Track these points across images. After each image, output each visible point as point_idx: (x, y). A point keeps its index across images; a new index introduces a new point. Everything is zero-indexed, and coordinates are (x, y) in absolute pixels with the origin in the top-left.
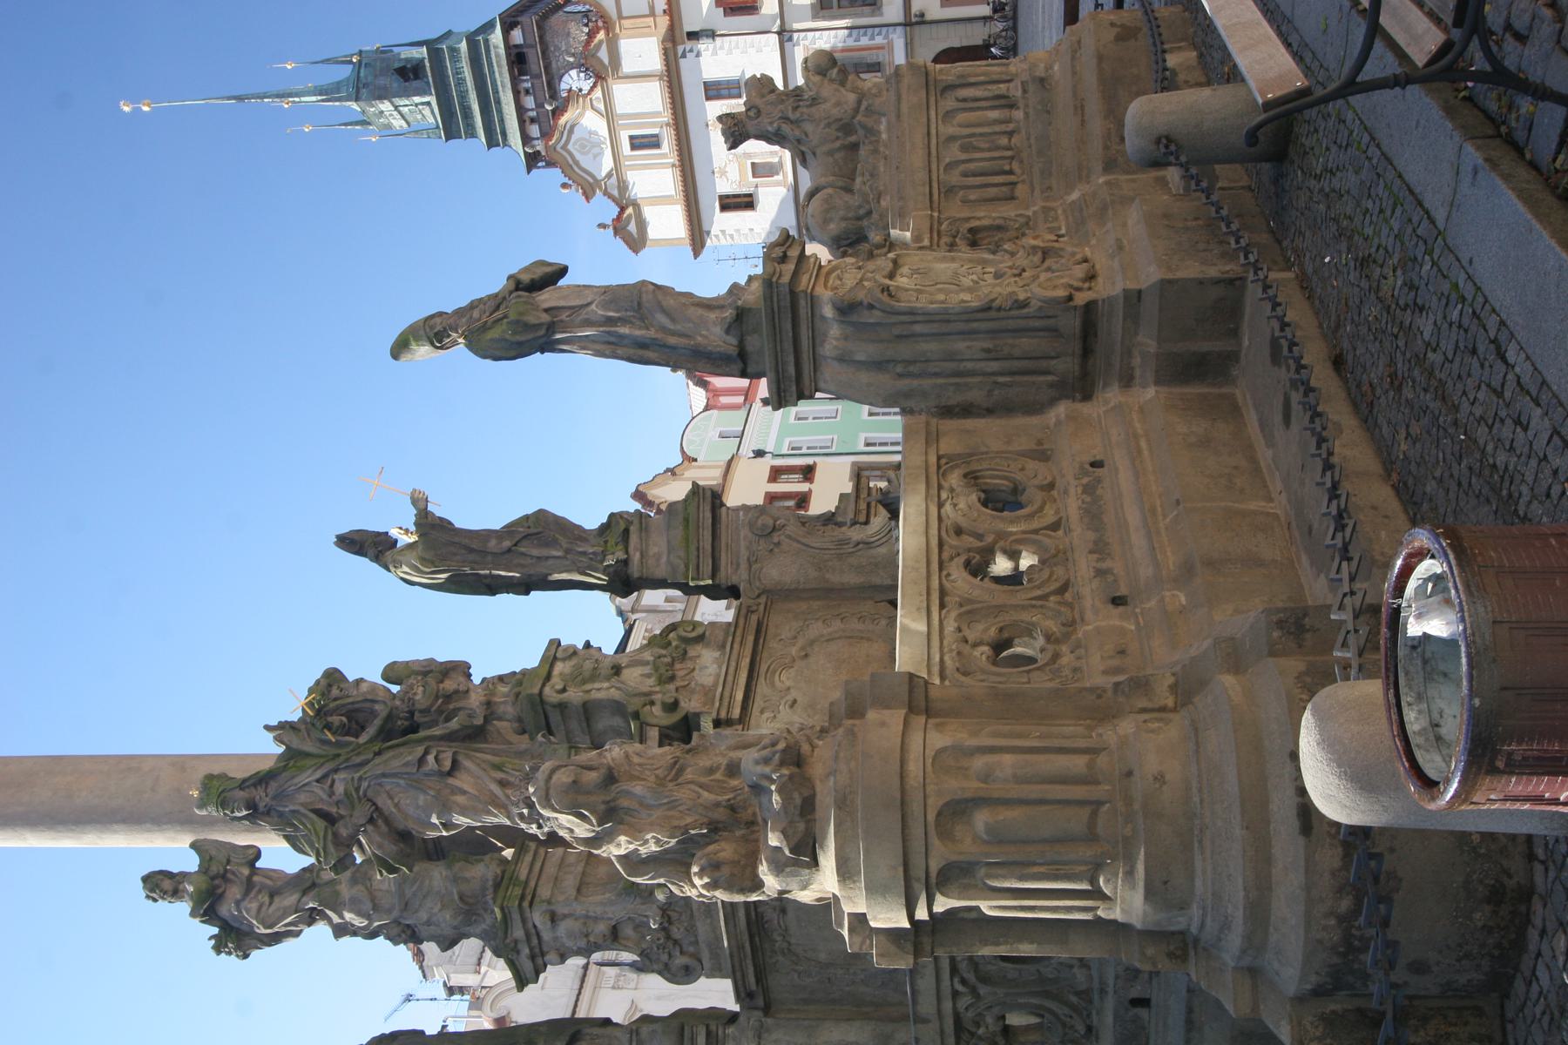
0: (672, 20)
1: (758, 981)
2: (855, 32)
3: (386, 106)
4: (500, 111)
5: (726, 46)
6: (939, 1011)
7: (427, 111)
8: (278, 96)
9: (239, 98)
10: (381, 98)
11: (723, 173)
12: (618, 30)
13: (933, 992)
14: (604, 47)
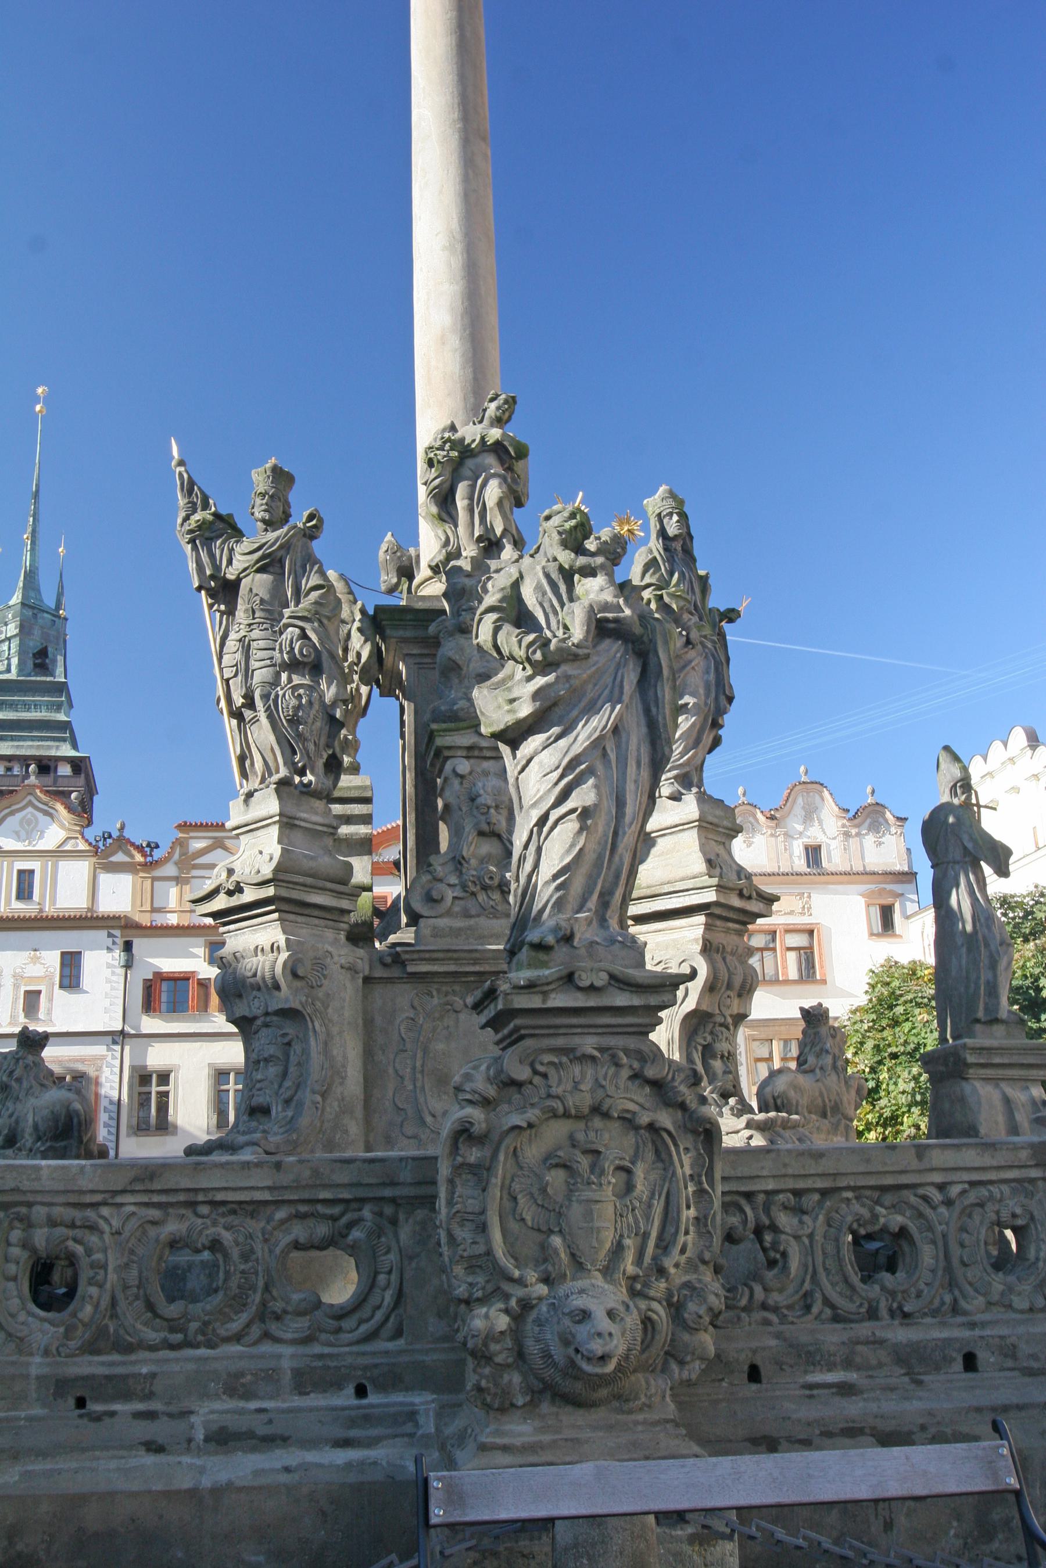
0: (146, 928)
2: (114, 1108)
5: (114, 978)
6: (932, 1170)
8: (34, 532)
9: (36, 495)
11: (35, 960)
12: (142, 874)
13: (962, 1164)
14: (127, 859)
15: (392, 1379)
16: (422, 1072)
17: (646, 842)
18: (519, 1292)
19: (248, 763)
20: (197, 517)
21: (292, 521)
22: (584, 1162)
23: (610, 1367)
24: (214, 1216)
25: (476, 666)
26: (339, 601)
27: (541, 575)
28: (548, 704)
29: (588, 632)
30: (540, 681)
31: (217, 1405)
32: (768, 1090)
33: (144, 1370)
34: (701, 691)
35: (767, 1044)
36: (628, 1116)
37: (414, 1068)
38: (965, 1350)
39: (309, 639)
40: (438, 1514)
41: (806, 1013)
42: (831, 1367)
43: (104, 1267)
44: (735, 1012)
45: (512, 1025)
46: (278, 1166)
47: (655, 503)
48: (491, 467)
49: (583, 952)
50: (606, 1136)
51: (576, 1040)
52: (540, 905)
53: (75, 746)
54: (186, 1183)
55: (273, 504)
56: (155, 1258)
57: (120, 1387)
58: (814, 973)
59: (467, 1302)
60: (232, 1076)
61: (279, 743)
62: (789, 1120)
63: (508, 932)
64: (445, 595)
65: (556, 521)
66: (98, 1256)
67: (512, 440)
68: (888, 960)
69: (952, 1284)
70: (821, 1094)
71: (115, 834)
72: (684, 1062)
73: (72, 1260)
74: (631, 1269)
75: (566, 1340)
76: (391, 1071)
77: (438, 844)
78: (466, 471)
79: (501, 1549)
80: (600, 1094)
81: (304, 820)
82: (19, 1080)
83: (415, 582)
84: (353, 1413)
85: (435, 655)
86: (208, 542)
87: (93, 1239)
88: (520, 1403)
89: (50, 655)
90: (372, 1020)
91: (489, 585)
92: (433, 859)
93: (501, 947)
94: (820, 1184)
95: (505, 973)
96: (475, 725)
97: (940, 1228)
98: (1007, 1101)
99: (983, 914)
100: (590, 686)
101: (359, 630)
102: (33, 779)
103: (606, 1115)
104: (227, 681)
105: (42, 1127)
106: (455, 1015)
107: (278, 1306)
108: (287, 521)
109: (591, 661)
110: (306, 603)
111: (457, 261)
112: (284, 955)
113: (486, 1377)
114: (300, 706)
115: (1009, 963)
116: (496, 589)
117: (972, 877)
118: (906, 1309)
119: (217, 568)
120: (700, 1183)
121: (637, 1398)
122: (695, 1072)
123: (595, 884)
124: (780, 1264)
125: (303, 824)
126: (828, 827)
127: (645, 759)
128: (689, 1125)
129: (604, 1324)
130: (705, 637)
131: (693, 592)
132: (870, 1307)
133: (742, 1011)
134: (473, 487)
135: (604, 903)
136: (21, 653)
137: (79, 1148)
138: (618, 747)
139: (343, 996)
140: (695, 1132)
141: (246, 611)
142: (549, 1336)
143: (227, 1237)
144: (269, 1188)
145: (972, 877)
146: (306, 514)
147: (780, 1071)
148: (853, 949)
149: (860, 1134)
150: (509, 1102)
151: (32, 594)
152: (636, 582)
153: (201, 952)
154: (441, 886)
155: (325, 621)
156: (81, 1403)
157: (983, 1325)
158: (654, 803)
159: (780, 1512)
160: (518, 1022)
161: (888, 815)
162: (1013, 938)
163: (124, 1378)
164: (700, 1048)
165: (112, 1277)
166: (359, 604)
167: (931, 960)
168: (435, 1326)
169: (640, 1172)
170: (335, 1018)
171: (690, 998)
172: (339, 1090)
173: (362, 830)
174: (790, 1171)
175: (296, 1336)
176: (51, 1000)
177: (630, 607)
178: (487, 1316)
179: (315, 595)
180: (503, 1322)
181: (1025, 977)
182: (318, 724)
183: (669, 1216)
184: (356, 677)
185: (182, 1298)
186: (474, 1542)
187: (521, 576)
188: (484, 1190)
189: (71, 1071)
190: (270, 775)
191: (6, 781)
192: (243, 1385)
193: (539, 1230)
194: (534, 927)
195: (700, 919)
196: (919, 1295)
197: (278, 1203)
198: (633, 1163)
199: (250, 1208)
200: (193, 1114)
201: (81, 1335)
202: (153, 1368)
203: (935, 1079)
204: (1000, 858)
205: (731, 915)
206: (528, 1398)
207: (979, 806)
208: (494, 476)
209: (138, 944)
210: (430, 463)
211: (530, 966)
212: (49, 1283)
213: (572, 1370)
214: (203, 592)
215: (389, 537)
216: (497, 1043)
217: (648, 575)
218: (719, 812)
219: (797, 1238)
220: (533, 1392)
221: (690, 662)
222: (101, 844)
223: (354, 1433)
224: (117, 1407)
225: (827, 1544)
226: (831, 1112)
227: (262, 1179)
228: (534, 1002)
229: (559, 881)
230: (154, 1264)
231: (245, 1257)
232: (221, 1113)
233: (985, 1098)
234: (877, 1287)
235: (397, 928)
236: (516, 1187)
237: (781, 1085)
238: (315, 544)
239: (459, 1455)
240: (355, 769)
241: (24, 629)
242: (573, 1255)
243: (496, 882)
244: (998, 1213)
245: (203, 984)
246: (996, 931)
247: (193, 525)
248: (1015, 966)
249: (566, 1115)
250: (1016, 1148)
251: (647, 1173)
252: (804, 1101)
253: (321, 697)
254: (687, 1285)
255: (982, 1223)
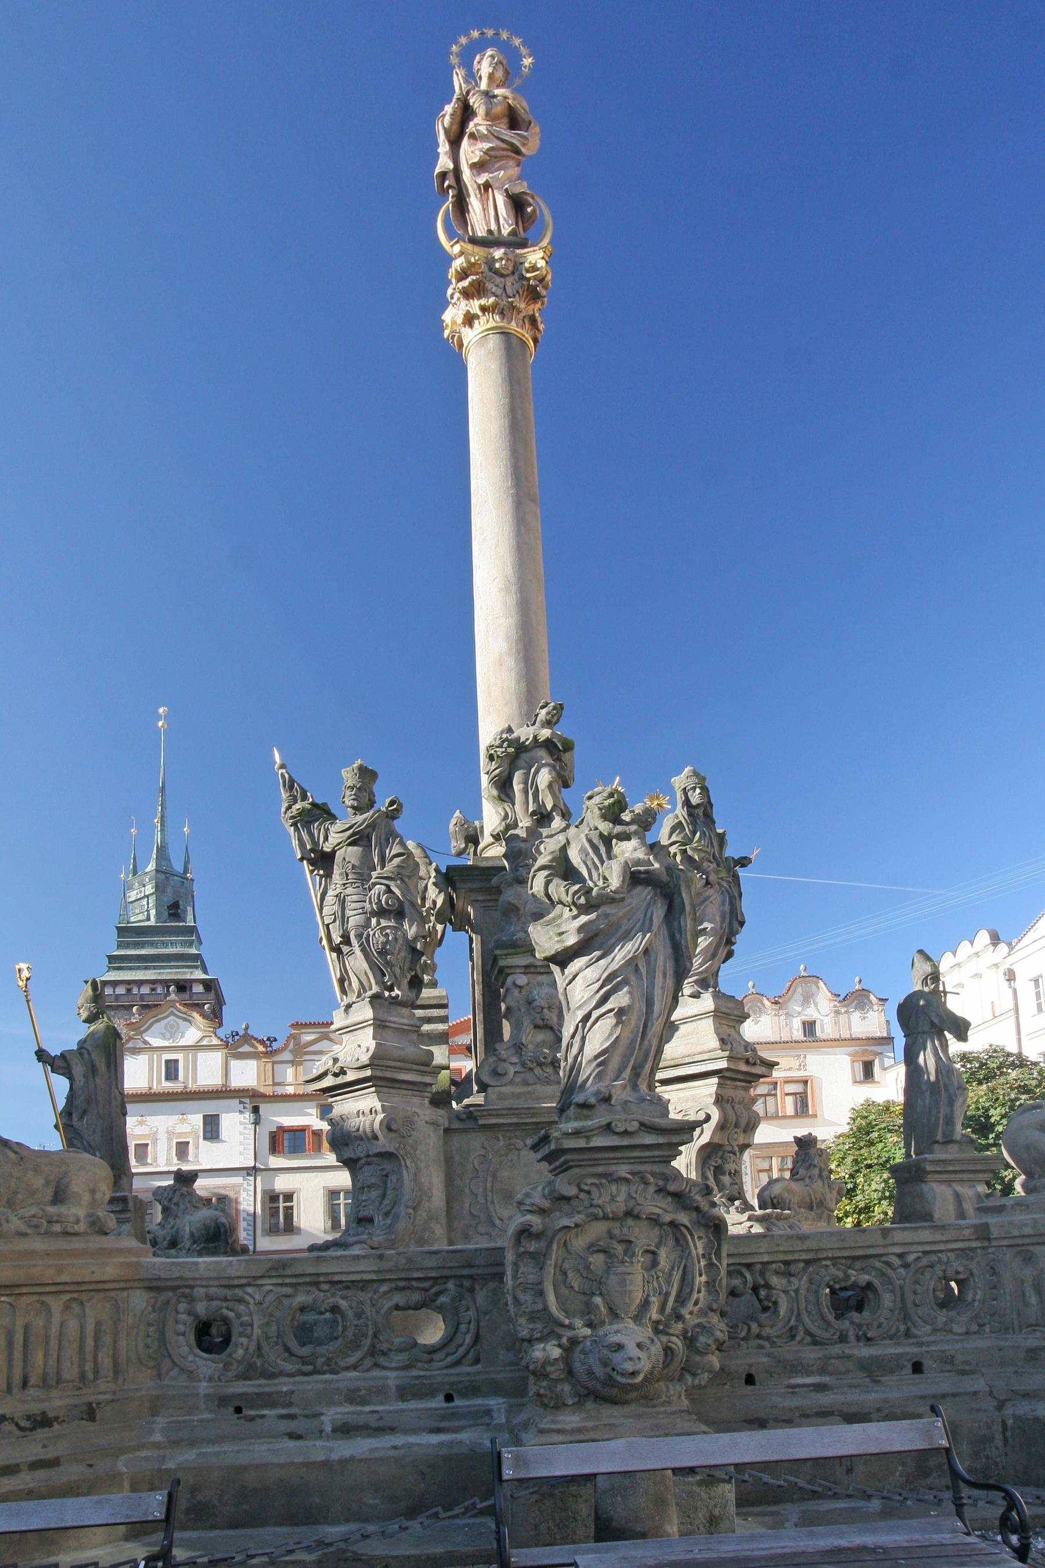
0: (269, 1096)
1: (484, 1126)
2: (251, 1218)
3: (149, 889)
4: (138, 968)
5: (246, 1131)
7: (141, 917)
8: (162, 817)
10: (157, 887)
11: (183, 1121)
13: (917, 1240)
15: (472, 1390)
16: (492, 1191)
17: (671, 1028)
18: (570, 1333)
19: (346, 984)
20: (298, 806)
21: (376, 807)
22: (619, 1249)
23: (639, 1379)
24: (333, 1290)
25: (531, 907)
26: (417, 865)
27: (584, 840)
28: (589, 935)
29: (623, 881)
30: (584, 919)
31: (341, 1409)
32: (766, 1193)
33: (285, 1389)
34: (718, 919)
35: (768, 1160)
36: (655, 1217)
37: (485, 1189)
38: (915, 1360)
39: (394, 893)
40: (508, 1473)
41: (798, 1141)
42: (810, 1374)
43: (252, 1325)
44: (741, 1143)
45: (562, 1160)
46: (381, 1257)
47: (681, 780)
48: (542, 758)
49: (619, 1108)
50: (637, 1230)
51: (614, 1168)
52: (584, 1077)
53: (205, 972)
54: (311, 1270)
55: (360, 795)
56: (290, 1318)
57: (269, 1400)
58: (808, 1110)
59: (529, 1341)
60: (342, 1194)
61: (371, 969)
62: (782, 1214)
63: (559, 1094)
64: (505, 856)
65: (597, 799)
66: (246, 1318)
67: (560, 737)
68: (867, 1100)
69: (906, 1317)
70: (809, 1195)
71: (241, 1033)
72: (700, 1180)
73: (226, 1321)
74: (655, 1316)
75: (605, 1363)
76: (467, 1191)
77: (502, 1035)
78: (521, 762)
79: (556, 1492)
80: (632, 1203)
81: (394, 1023)
82: (177, 1204)
83: (480, 847)
84: (443, 1412)
85: (497, 900)
86: (307, 825)
87: (242, 1308)
88: (570, 1403)
89: (181, 907)
90: (452, 1158)
91: (542, 848)
92: (497, 1046)
93: (554, 1105)
94: (804, 1256)
95: (556, 1123)
96: (532, 951)
97: (898, 1283)
98: (957, 1196)
99: (944, 1068)
100: (625, 921)
101: (434, 884)
102: (173, 996)
103: (637, 1217)
104: (328, 925)
105: (196, 1234)
106: (516, 1153)
107: (384, 1347)
108: (372, 806)
109: (626, 902)
110: (390, 867)
111: (512, 600)
112: (381, 1116)
113: (544, 1387)
114: (387, 942)
115: (965, 1101)
116: (547, 852)
117: (936, 1042)
118: (869, 1335)
119: (315, 843)
120: (710, 1259)
121: (659, 1397)
122: (707, 1186)
123: (629, 1061)
124: (772, 1309)
125: (392, 1025)
126: (822, 1008)
127: (670, 972)
128: (702, 1222)
129: (635, 1352)
130: (722, 879)
131: (712, 846)
132: (841, 1335)
133: (746, 1142)
134: (527, 774)
135: (636, 1073)
136: (158, 906)
137: (225, 1248)
138: (648, 964)
139: (428, 1143)
140: (706, 1226)
141: (341, 874)
142: (592, 1361)
143: (343, 1304)
144: (374, 1271)
145: (936, 1042)
146: (388, 801)
147: (777, 1180)
148: (839, 1090)
149: (840, 1219)
150: (561, 1211)
151: (164, 863)
152: (665, 842)
153: (314, 1111)
154: (505, 1065)
155: (406, 879)
156: (238, 1410)
157: (928, 1344)
158: (677, 1002)
159: (766, 1466)
160: (568, 1157)
161: (872, 997)
162: (968, 1082)
163: (270, 1394)
164: (712, 1168)
165: (257, 1331)
166: (434, 865)
167: (901, 1099)
168: (504, 1356)
169: (662, 1253)
170: (422, 1157)
171: (704, 1136)
172: (427, 1205)
173: (441, 1027)
174: (781, 1249)
175: (400, 1364)
176: (197, 1148)
177: (658, 862)
178: (544, 1349)
179: (397, 861)
180: (556, 1353)
181: (978, 1109)
182: (403, 954)
183: (686, 1281)
184: (432, 918)
185: (311, 1343)
186: (536, 1489)
187: (568, 842)
188: (541, 1269)
189: (216, 1195)
190: (365, 991)
191: (152, 998)
192: (359, 1396)
193: (584, 1293)
194: (580, 1092)
195: (715, 1080)
196: (879, 1326)
197: (382, 1281)
198: (657, 1248)
199: (361, 1285)
200: (313, 1220)
201: (235, 1369)
202: (291, 1387)
203: (899, 1183)
204: (961, 1028)
205: (739, 1077)
206: (576, 1400)
207: (945, 993)
208: (544, 765)
209: (263, 1108)
210: (491, 758)
211: (576, 1119)
212: (209, 1335)
213: (610, 1381)
214: (305, 862)
215: (457, 813)
216: (551, 1171)
217: (674, 835)
218: (730, 1005)
219: (785, 1292)
220: (580, 1396)
221: (709, 897)
222: (230, 1040)
223: (443, 1424)
224: (266, 1412)
225: (801, 1483)
226: (818, 1206)
227: (370, 1265)
228: (581, 1143)
229: (599, 1060)
230: (288, 1322)
231: (359, 1316)
232: (335, 1226)
233: (940, 1196)
234: (847, 1322)
235: (470, 1094)
236: (566, 1266)
237: (777, 1189)
238: (396, 823)
239: (524, 1436)
240: (433, 984)
241: (159, 889)
242: (610, 1309)
243: (549, 1060)
244: (944, 1271)
245: (317, 1134)
246: (955, 1080)
247: (295, 812)
248: (969, 1101)
249: (605, 1218)
250: (961, 1228)
251: (668, 1254)
252: (795, 1200)
253: (405, 934)
254: (699, 1325)
255: (931, 1278)
